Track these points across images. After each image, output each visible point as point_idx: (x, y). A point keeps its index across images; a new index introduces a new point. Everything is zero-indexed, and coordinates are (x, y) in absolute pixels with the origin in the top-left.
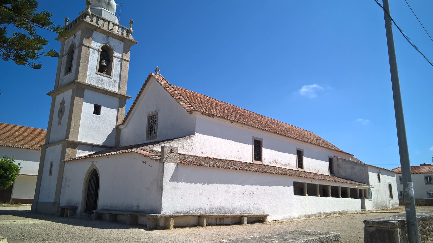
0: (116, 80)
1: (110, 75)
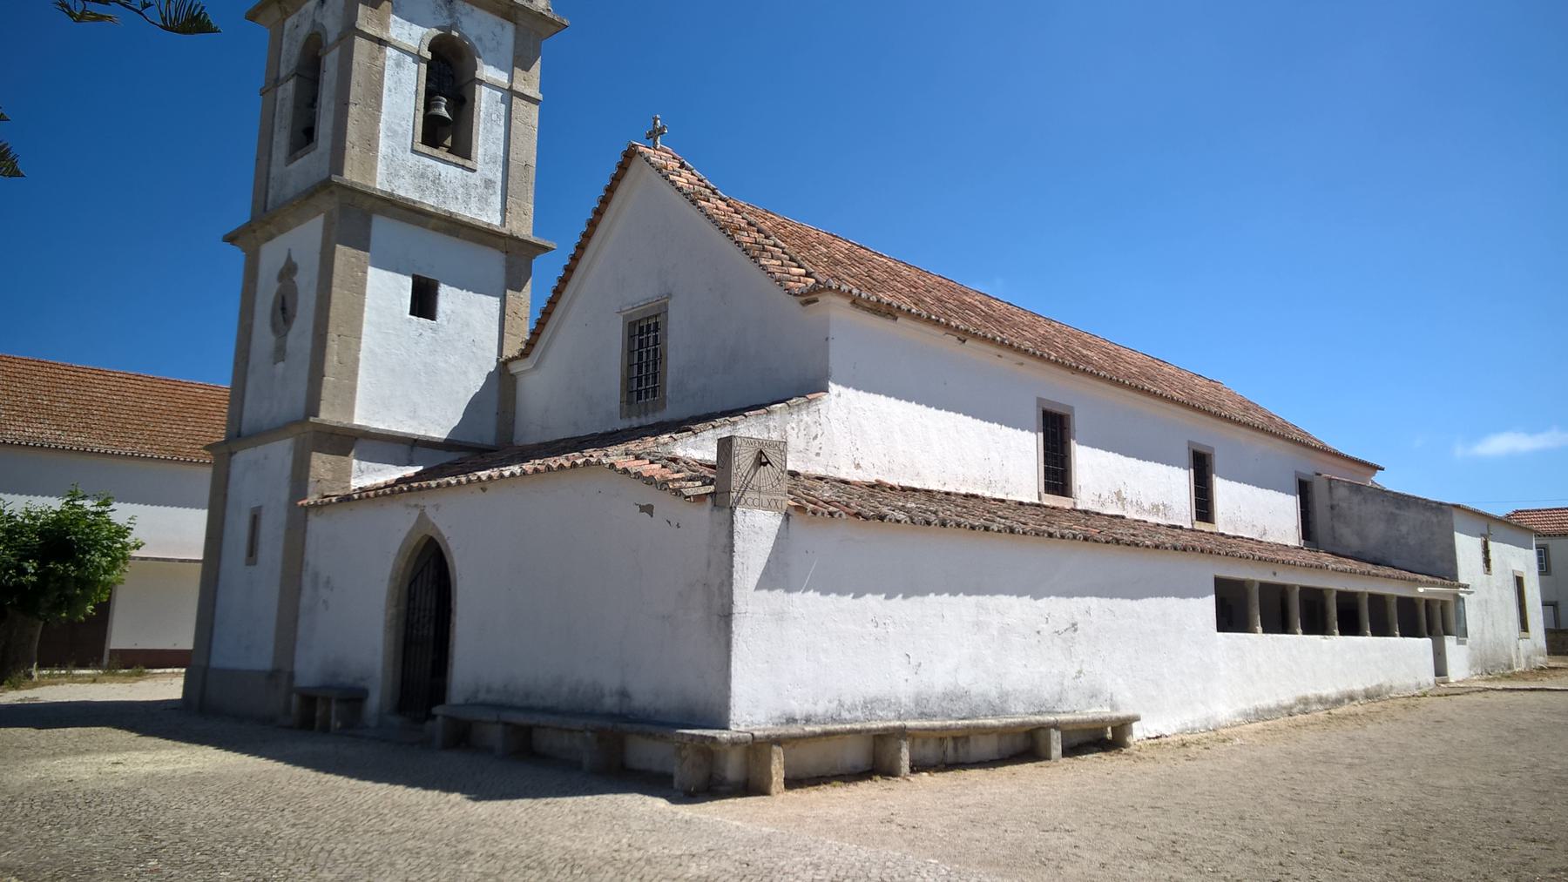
0: (491, 176)
1: (469, 158)
